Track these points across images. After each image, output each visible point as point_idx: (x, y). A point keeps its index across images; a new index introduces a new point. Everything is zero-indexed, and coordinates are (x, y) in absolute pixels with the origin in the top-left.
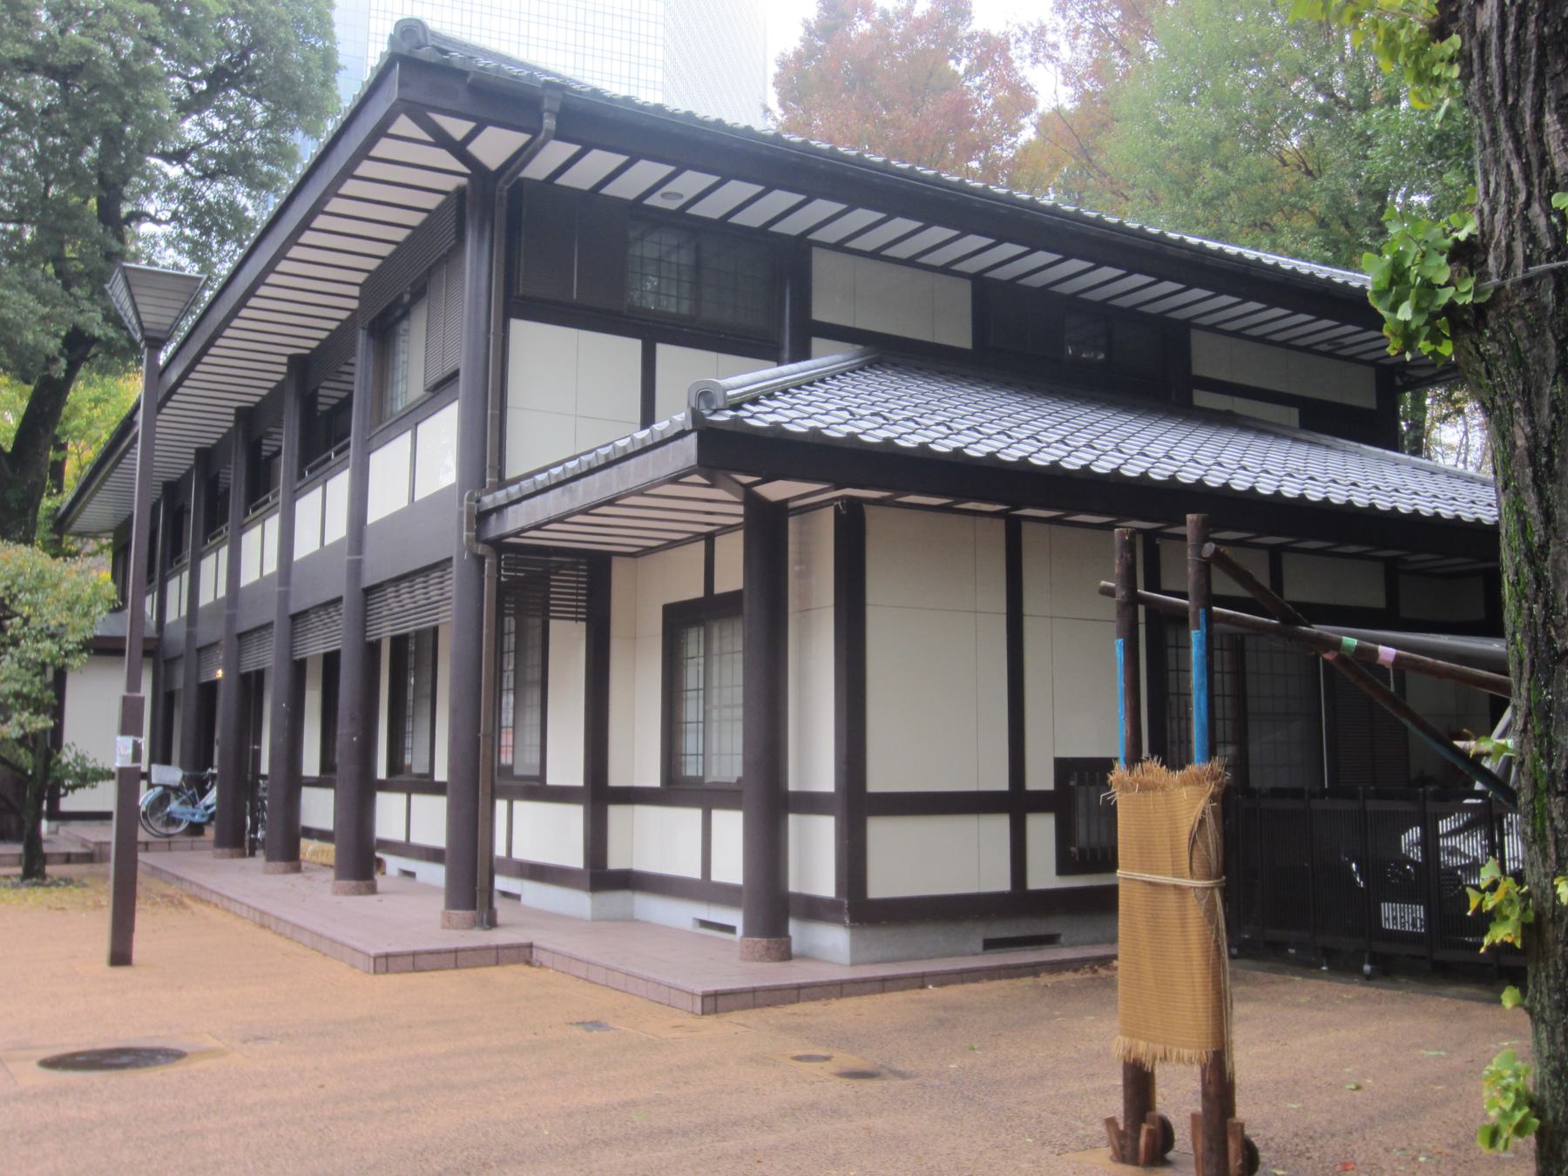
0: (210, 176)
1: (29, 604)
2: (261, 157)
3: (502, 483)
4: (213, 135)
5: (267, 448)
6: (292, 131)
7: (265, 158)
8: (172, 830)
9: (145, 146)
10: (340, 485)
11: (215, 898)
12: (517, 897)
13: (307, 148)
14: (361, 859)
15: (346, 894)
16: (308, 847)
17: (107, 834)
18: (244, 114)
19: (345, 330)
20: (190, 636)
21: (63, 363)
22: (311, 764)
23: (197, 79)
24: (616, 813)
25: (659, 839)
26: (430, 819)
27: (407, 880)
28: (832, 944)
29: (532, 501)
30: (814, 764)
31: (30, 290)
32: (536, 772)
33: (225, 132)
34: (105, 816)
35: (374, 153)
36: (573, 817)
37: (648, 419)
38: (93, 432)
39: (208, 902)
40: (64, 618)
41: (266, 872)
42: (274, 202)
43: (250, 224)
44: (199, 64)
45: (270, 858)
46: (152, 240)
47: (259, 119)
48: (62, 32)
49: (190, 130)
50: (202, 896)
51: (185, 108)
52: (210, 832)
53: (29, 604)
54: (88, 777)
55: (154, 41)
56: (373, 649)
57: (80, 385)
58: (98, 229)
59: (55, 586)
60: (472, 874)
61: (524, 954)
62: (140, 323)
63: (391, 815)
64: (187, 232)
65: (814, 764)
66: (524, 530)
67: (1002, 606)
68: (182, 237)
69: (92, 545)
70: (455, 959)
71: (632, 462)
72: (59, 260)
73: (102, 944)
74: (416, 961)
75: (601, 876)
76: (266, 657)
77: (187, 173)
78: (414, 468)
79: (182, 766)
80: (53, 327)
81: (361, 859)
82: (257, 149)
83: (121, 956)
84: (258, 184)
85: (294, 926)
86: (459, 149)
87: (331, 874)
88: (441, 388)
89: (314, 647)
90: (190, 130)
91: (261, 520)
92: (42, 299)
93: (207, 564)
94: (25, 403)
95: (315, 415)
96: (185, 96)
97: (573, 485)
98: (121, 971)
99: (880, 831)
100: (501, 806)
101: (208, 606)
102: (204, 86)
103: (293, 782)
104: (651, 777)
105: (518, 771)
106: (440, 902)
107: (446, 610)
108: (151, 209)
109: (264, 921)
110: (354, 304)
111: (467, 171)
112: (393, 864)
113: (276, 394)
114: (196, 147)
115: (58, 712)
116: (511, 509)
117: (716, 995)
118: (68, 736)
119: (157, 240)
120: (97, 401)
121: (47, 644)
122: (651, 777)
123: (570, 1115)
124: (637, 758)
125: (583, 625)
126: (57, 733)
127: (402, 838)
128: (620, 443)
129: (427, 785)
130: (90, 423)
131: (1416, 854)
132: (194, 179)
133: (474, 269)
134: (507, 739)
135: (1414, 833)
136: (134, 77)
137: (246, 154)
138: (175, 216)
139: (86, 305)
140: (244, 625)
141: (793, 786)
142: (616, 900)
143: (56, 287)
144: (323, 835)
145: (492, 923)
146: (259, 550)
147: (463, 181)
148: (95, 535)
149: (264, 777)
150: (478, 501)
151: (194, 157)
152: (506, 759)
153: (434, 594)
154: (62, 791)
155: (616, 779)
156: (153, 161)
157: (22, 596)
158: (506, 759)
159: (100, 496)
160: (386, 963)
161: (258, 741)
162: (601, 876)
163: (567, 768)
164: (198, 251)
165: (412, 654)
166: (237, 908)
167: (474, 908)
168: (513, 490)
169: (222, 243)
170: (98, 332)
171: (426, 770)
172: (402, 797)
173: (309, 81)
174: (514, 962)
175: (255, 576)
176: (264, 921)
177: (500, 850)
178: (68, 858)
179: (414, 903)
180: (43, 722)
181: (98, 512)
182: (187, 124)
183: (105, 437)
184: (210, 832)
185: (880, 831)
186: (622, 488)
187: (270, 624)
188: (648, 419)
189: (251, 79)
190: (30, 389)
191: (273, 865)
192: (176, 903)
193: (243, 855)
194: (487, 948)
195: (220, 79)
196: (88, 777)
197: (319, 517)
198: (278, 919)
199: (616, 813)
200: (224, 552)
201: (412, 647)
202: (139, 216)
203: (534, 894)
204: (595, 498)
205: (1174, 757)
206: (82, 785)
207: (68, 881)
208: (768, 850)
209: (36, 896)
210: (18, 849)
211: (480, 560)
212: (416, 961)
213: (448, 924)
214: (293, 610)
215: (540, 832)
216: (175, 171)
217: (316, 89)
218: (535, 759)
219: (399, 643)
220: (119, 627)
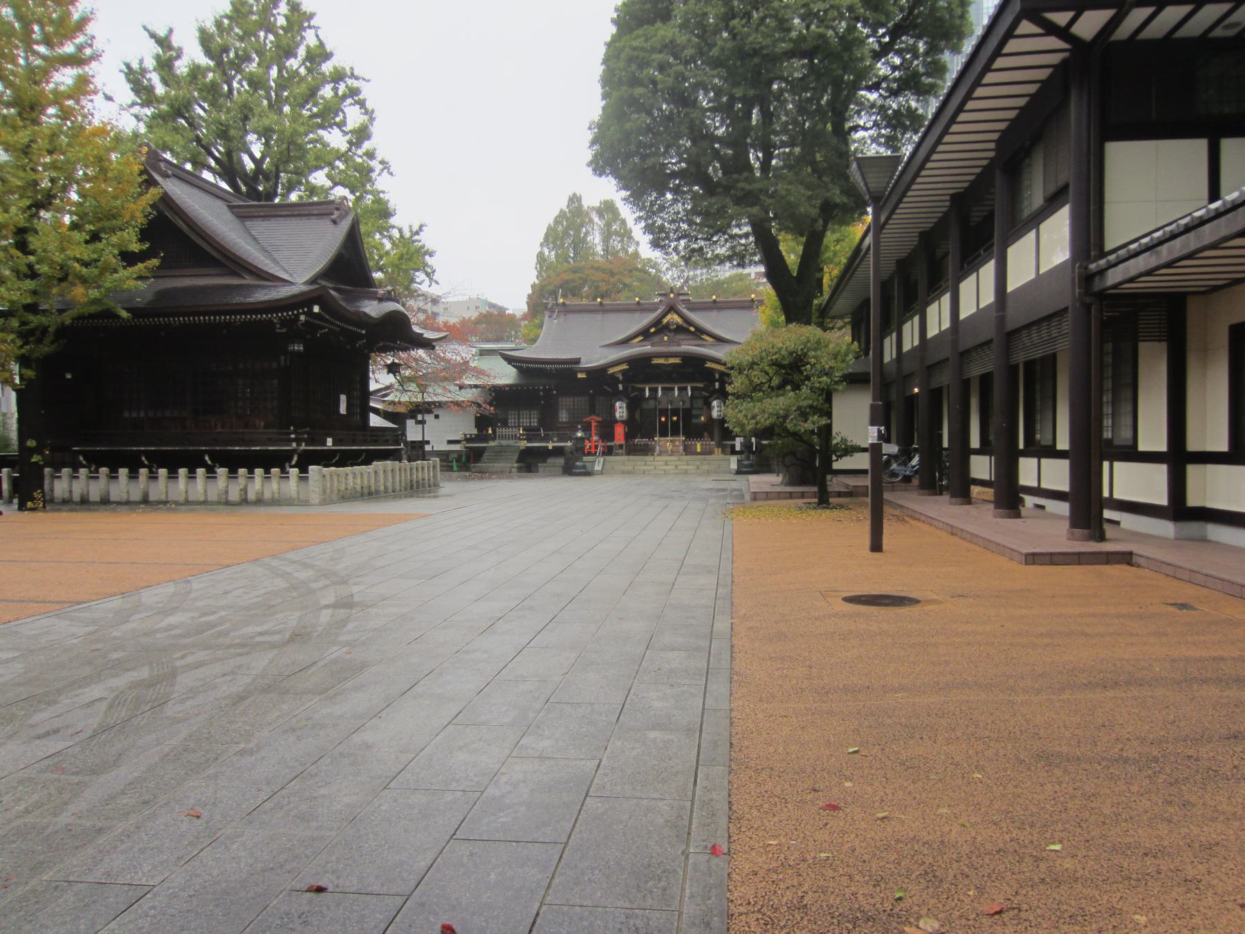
0: (894, 93)
1: (815, 357)
2: (923, 74)
3: (1103, 254)
4: (894, 68)
5: (939, 253)
6: (942, 52)
7: (928, 74)
8: (894, 480)
9: (855, 86)
10: (988, 271)
11: (923, 518)
12: (1118, 523)
13: (954, 63)
14: (1009, 497)
15: (1002, 517)
16: (975, 490)
17: (866, 481)
18: (913, 50)
19: (987, 172)
20: (899, 369)
21: (821, 222)
22: (975, 442)
23: (883, 35)
24: (1193, 471)
26: (1057, 475)
27: (1040, 511)
29: (1127, 263)
31: (801, 183)
32: (1130, 443)
33: (901, 64)
34: (864, 472)
35: (1005, 51)
36: (1159, 474)
37: (1214, 194)
38: (837, 260)
39: (919, 520)
40: (832, 363)
41: (951, 504)
42: (934, 104)
43: (922, 117)
44: (882, 25)
45: (952, 496)
46: (862, 141)
47: (921, 50)
48: (808, 28)
49: (882, 69)
50: (915, 516)
51: (877, 56)
52: (916, 482)
53: (815, 357)
54: (850, 450)
55: (857, 19)
56: (1013, 370)
57: (828, 233)
58: (834, 141)
59: (826, 346)
60: (1088, 506)
61: (1126, 558)
62: (868, 189)
63: (1028, 471)
64: (883, 131)
66: (1121, 283)
68: (880, 136)
69: (840, 323)
70: (1078, 559)
71: (1207, 227)
72: (813, 163)
73: (866, 540)
74: (1052, 559)
75: (1179, 509)
76: (944, 378)
77: (881, 95)
78: (1042, 252)
79: (898, 444)
80: (814, 202)
81: (1009, 497)
82: (921, 70)
83: (876, 546)
84: (923, 92)
85: (972, 534)
86: (1063, 33)
87: (992, 506)
88: (1053, 203)
89: (975, 370)
90: (882, 69)
91: (938, 297)
92: (808, 187)
93: (907, 327)
94: (801, 248)
95: (975, 225)
96: (876, 47)
97: (1159, 249)
98: (877, 555)
100: (1106, 465)
101: (909, 352)
102: (887, 39)
103: (965, 452)
105: (1116, 443)
106: (1067, 524)
107: (1063, 344)
108: (861, 123)
109: (953, 531)
110: (992, 154)
111: (1066, 46)
112: (1030, 501)
113: (942, 222)
114: (885, 78)
115: (829, 415)
116: (1110, 271)
117: (1034, 554)
118: (835, 430)
119: (866, 139)
120: (838, 241)
121: (825, 378)
123: (1174, 661)
124: (1211, 426)
125: (1164, 345)
126: (829, 427)
127: (1035, 484)
128: (1197, 214)
129: (1051, 452)
130: (835, 254)
132: (885, 98)
133: (1076, 112)
134: (1108, 422)
136: (850, 42)
137: (916, 75)
138: (876, 124)
139: (831, 186)
140: (930, 361)
142: (1193, 528)
143: (814, 179)
144: (982, 483)
145: (1101, 538)
146: (938, 317)
147: (1066, 54)
148: (841, 317)
149: (946, 449)
150: (1086, 268)
151: (884, 85)
152: (1107, 434)
153: (1054, 333)
154: (834, 458)
155: (1193, 445)
156: (863, 93)
157: (812, 353)
158: (1107, 434)
159: (845, 294)
160: (1033, 559)
161: (941, 428)
162: (1179, 509)
163: (1153, 437)
164: (891, 142)
165: (1039, 375)
166: (936, 523)
167: (1089, 528)
168: (1112, 257)
169: (903, 134)
170: (838, 200)
171: (1050, 443)
172: (1035, 460)
173: (952, 17)
174: (1119, 563)
175: (937, 332)
176: (953, 531)
177: (1106, 494)
178: (839, 494)
179: (1050, 525)
180: (824, 421)
181: (843, 304)
182: (879, 65)
183: (844, 261)
184: (916, 482)
186: (1199, 245)
187: (947, 359)
188: (1214, 194)
189: (916, 26)
190: (804, 239)
191: (954, 500)
192: (900, 519)
193: (935, 494)
194: (1100, 553)
195: (895, 33)
196: (850, 450)
197: (976, 292)
198: (962, 530)
199: (1193, 471)
200: (916, 319)
201: (1038, 368)
202: (856, 128)
203: (1128, 521)
204: (1177, 255)
206: (845, 455)
207: (841, 506)
209: (826, 514)
210: (815, 489)
211: (1087, 307)
212: (1052, 559)
213: (1072, 537)
214: (961, 349)
216: (873, 96)
217: (958, 22)
218: (1050, 437)
219: (1029, 365)
220: (868, 365)
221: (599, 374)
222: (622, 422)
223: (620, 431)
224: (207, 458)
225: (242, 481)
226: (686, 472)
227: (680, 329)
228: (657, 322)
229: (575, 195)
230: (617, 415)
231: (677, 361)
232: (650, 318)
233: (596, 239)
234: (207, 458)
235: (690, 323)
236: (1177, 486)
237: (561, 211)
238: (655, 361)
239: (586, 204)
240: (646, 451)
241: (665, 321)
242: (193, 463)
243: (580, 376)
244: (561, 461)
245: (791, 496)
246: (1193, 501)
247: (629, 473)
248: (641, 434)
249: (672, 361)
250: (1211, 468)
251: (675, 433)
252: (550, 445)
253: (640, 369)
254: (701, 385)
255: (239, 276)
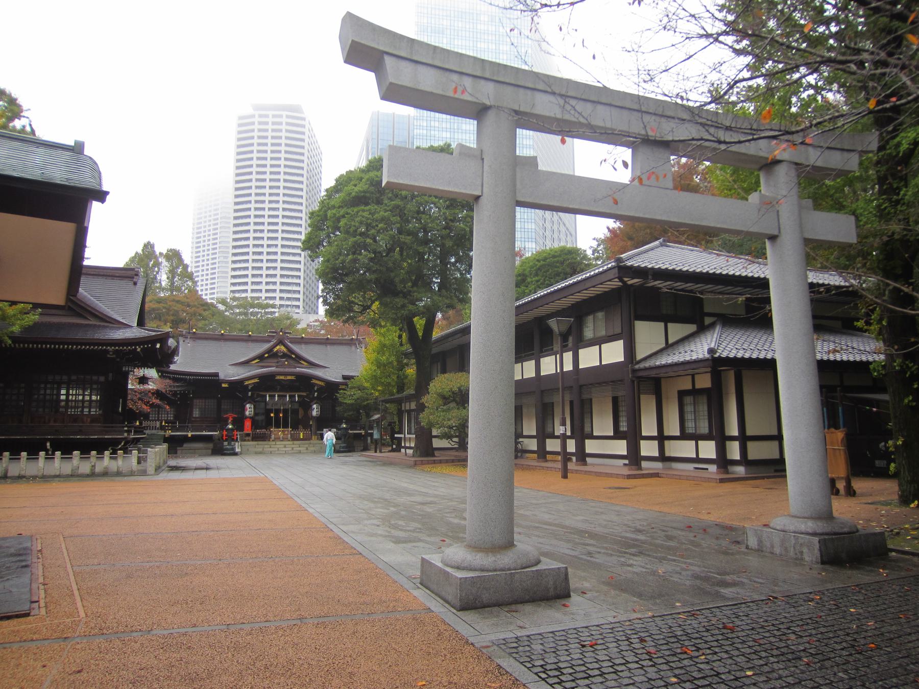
24: (667, 443)
25: (686, 449)
28: (740, 470)
30: (733, 429)
65: (733, 429)
67: (774, 391)
75: (663, 457)
99: (750, 445)
104: (677, 433)
122: (677, 433)
124: (672, 427)
131: (884, 449)
135: (883, 444)
141: (727, 434)
142: (668, 464)
185: (750, 445)
199: (667, 443)
205: (837, 428)
208: (721, 450)
211: (633, 382)
215: (649, 449)
221: (237, 386)
222: (250, 418)
223: (248, 424)
224: (48, 444)
225: (93, 460)
226: (300, 452)
227: (284, 355)
228: (269, 351)
229: (149, 243)
230: (247, 413)
231: (293, 378)
232: (266, 346)
233: (163, 278)
234: (48, 444)
235: (292, 352)
236: (662, 448)
237: (137, 253)
238: (278, 377)
239: (158, 250)
240: (264, 438)
241: (275, 350)
242: (33, 450)
243: (223, 385)
244: (211, 445)
245: (422, 463)
246: (667, 454)
247: (260, 453)
248: (262, 429)
249: (289, 378)
250: (672, 442)
251: (285, 426)
252: (190, 434)
253: (267, 383)
254: (304, 394)
255: (86, 318)
